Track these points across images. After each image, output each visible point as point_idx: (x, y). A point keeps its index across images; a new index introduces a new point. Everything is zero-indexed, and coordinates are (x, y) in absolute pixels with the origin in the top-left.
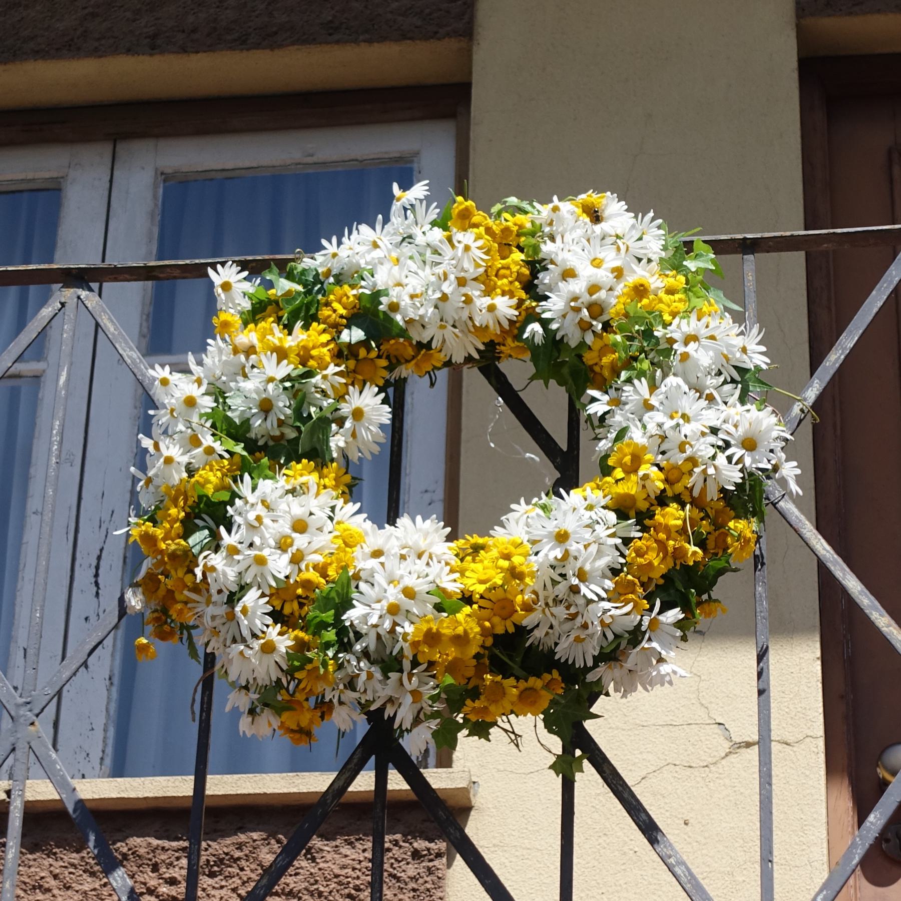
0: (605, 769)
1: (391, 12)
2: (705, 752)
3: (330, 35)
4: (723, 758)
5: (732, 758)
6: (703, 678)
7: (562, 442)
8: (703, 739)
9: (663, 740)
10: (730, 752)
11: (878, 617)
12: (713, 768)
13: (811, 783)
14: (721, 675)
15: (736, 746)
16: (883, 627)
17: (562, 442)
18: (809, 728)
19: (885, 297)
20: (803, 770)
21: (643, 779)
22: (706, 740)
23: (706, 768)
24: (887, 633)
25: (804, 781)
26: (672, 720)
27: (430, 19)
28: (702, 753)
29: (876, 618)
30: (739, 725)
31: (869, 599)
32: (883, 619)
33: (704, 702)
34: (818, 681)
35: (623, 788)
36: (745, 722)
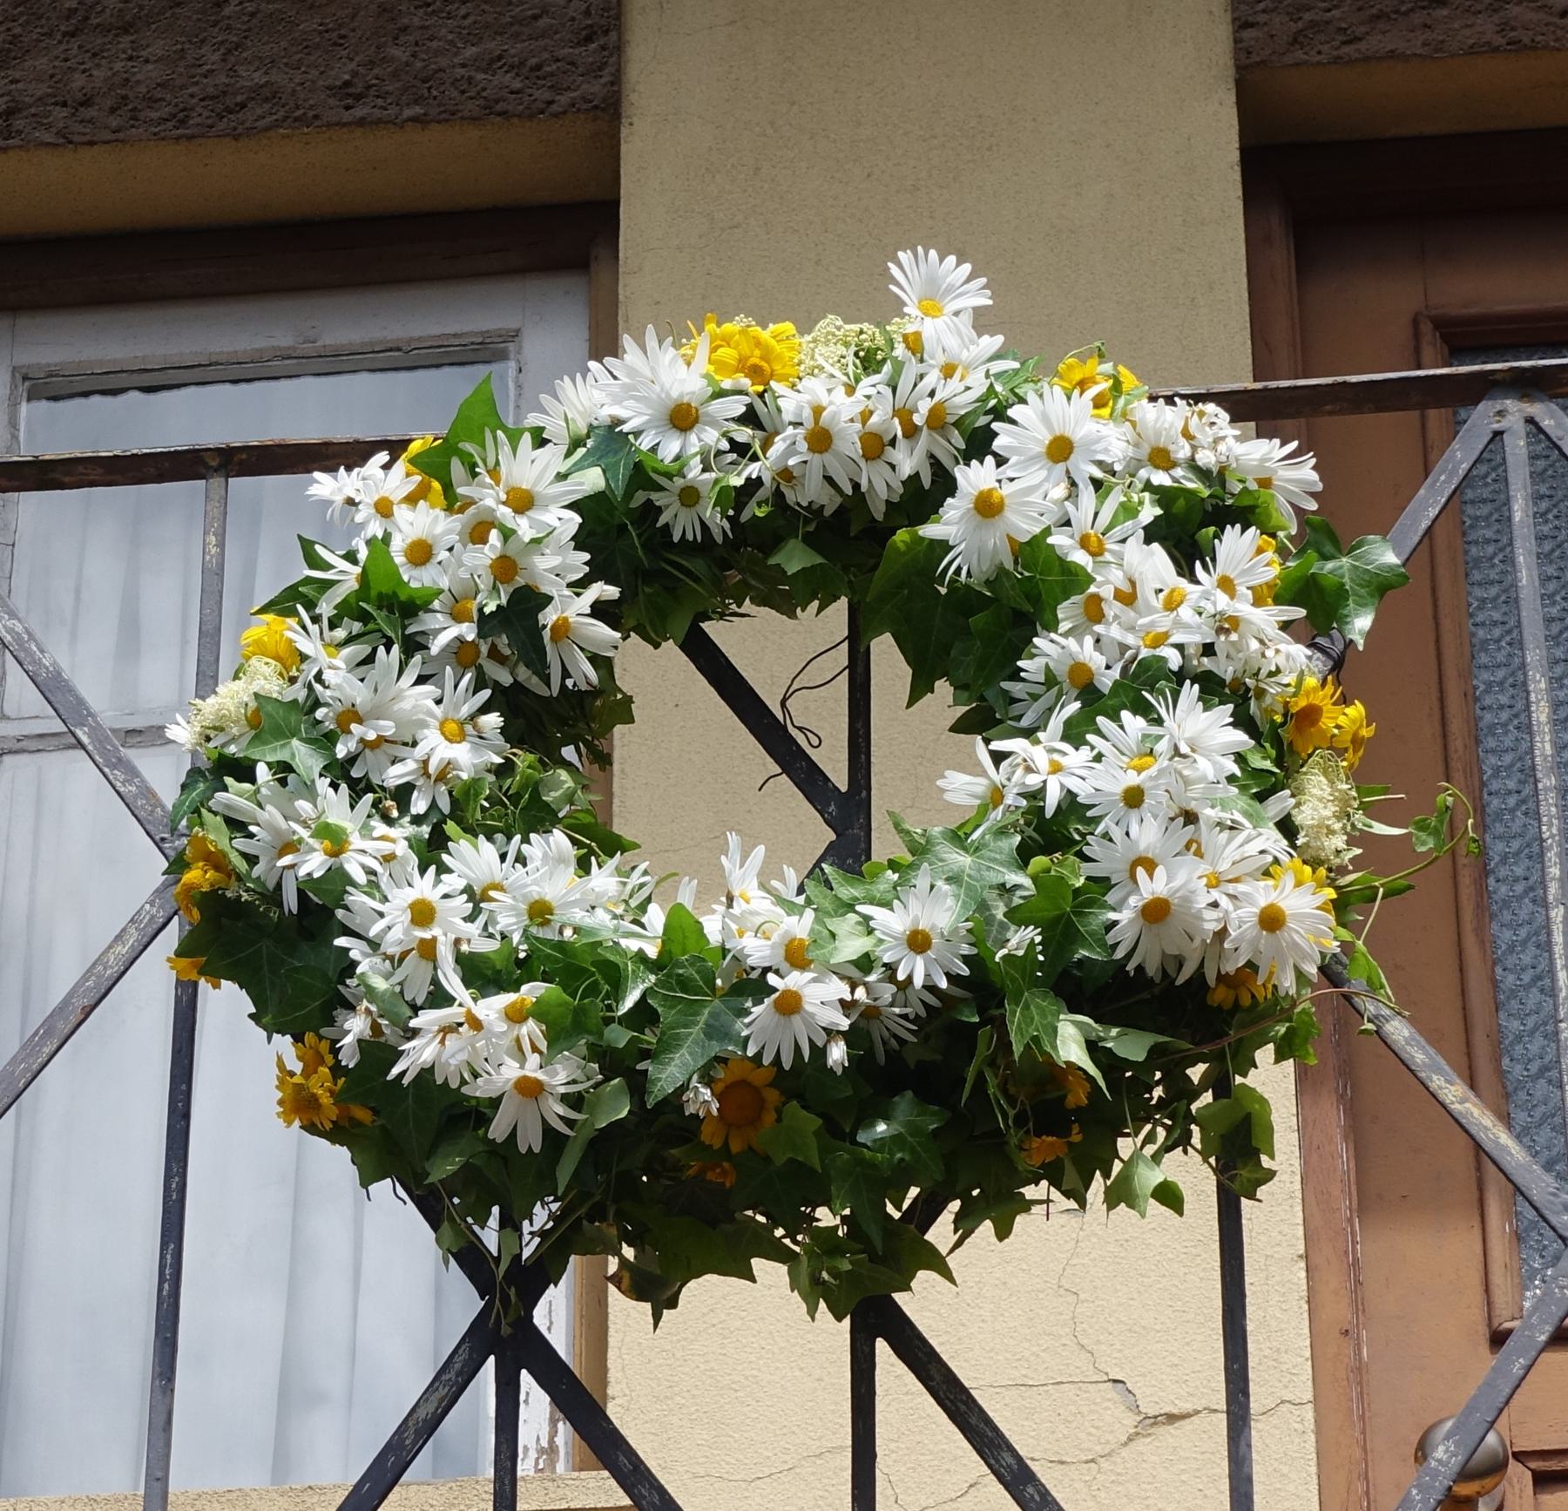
0: (933, 1372)
1: (463, 66)
2: (1089, 1434)
3: (348, 108)
4: (1125, 1444)
5: (1141, 1445)
6: (1082, 1296)
7: (839, 777)
8: (1085, 1410)
9: (1008, 1414)
10: (1138, 1434)
11: (1444, 1084)
12: (1104, 1464)
13: (1291, 1488)
14: (1117, 1291)
15: (1148, 1422)
16: (1453, 1103)
17: (839, 777)
18: (1286, 1387)
19: (1443, 500)
20: (1276, 1464)
21: (971, 1486)
22: (1091, 1411)
23: (1092, 1465)
24: (1461, 1113)
25: (1279, 1486)
26: (1025, 1376)
27: (538, 78)
28: (1083, 1436)
29: (1441, 1088)
30: (1153, 1382)
31: (1426, 1053)
32: (1452, 1088)
33: (1084, 1342)
34: (1302, 1298)
35: (968, 1407)
36: (1164, 1377)
